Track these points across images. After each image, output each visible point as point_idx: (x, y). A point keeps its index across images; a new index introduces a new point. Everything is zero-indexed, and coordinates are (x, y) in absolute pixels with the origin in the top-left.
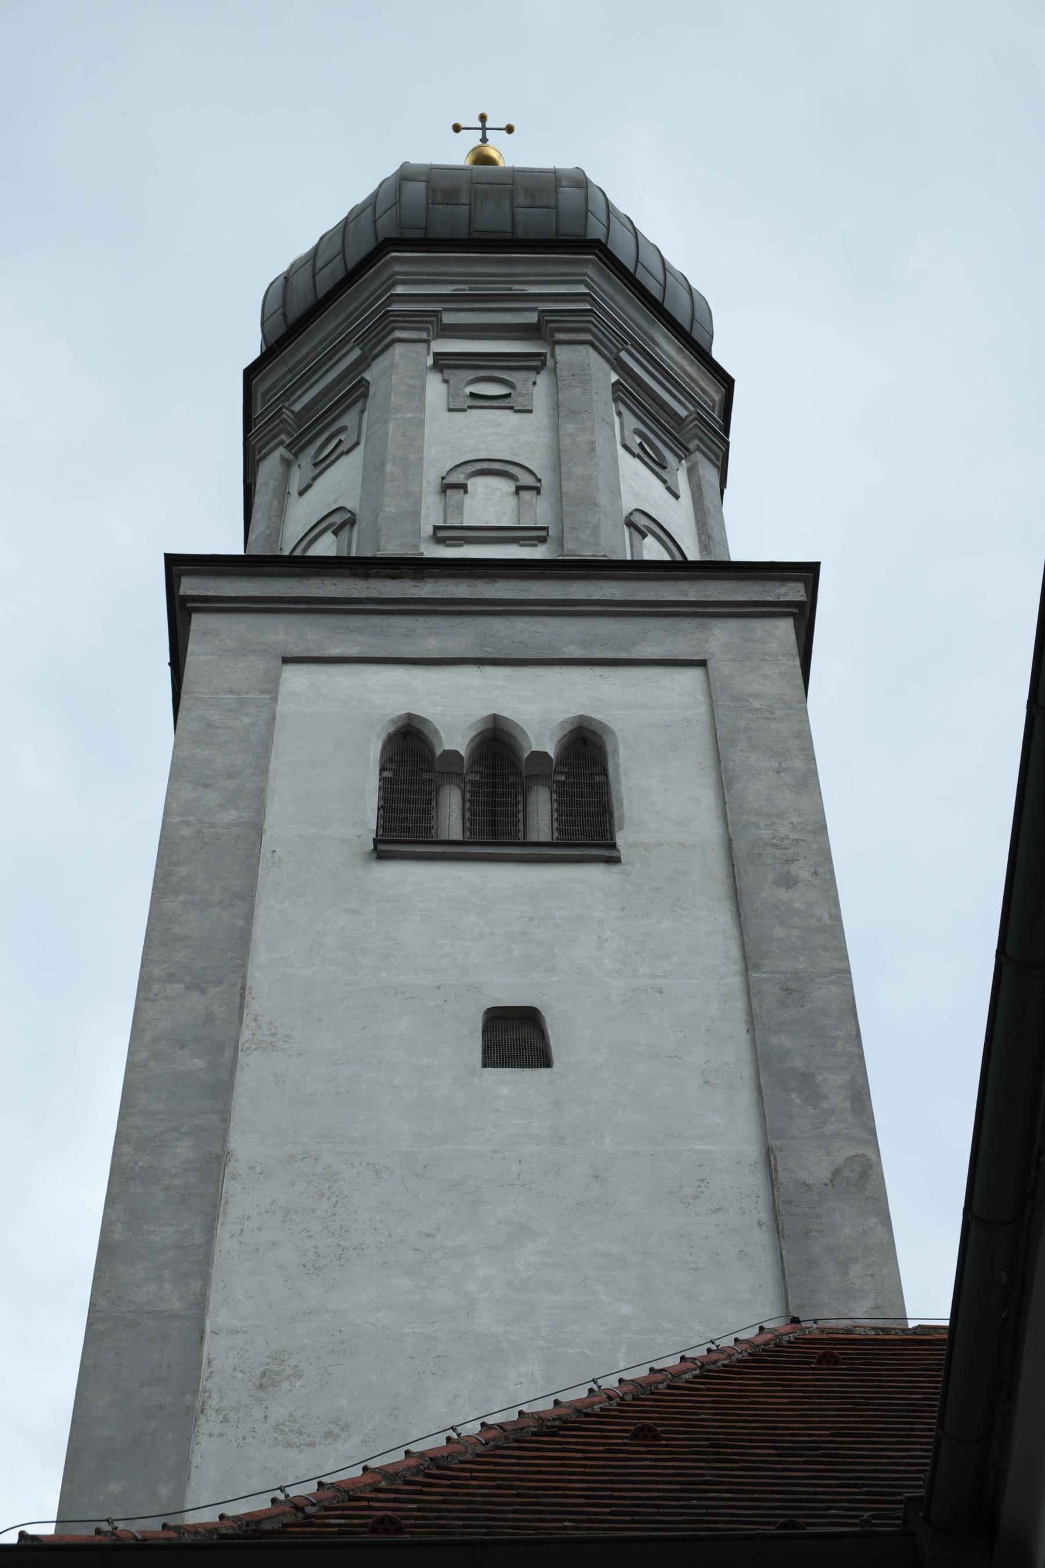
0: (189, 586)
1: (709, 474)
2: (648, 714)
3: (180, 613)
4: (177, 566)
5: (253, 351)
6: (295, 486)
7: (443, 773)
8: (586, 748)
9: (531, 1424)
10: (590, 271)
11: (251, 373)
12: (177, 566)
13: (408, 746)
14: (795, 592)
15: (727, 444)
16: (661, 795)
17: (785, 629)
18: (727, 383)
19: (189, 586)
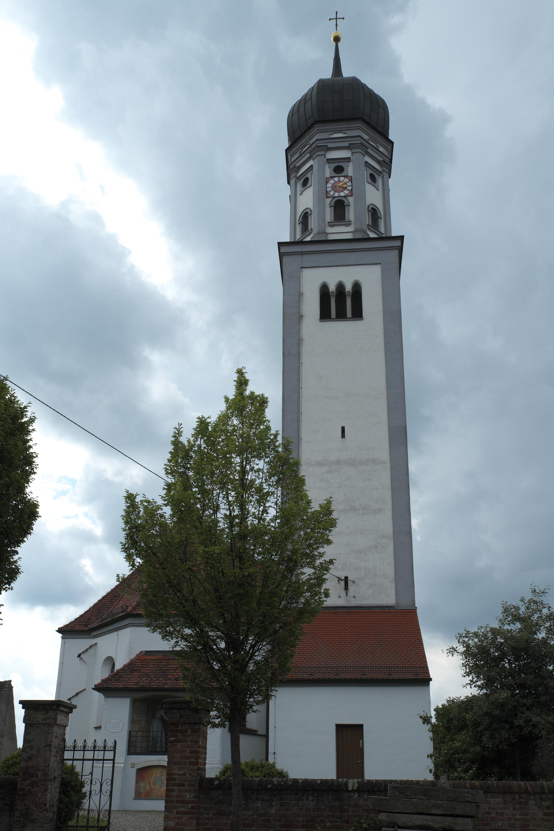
0: (284, 250)
1: (386, 176)
2: (368, 277)
3: (281, 255)
4: (280, 244)
5: (287, 146)
6: (298, 193)
7: (338, 462)
8: (357, 290)
9: (181, 684)
10: (360, 125)
11: (287, 151)
12: (280, 244)
13: (324, 291)
14: (398, 243)
15: (391, 166)
16: (372, 301)
17: (396, 253)
18: (392, 143)
19: (284, 250)
